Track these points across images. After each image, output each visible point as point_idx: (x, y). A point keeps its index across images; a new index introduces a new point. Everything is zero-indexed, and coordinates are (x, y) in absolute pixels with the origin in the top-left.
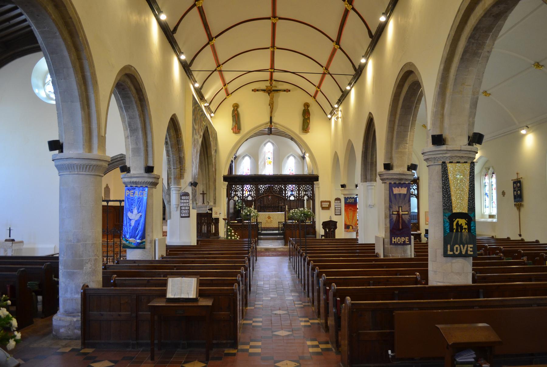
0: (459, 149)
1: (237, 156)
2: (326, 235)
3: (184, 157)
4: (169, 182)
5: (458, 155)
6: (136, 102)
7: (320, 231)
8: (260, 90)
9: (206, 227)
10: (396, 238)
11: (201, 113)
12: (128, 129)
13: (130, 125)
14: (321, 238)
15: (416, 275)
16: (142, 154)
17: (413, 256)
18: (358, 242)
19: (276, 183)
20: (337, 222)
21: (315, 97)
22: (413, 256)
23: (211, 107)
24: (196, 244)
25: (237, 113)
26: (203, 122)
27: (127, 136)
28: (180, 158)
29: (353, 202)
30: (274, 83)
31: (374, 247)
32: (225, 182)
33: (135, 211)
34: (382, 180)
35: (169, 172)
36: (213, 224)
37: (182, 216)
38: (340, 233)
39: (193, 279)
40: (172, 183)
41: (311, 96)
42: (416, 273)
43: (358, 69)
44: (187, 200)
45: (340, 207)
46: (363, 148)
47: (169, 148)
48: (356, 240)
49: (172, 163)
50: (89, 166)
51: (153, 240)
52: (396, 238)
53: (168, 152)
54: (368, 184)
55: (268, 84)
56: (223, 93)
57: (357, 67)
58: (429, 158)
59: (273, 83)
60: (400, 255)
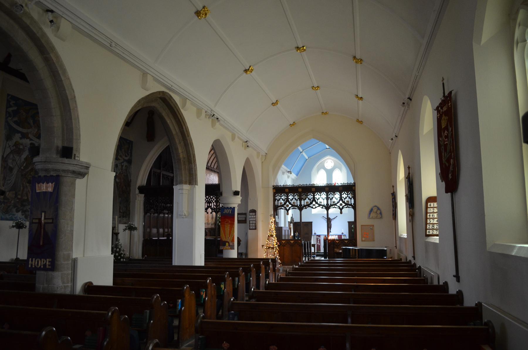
10: (34, 259)
29: (230, 213)
37: (250, 228)
44: (254, 216)
45: (255, 220)
52: (34, 259)
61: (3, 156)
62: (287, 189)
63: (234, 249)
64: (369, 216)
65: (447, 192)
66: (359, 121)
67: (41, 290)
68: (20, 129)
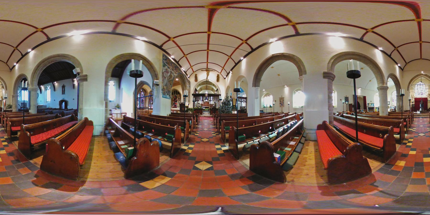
28: (156, 74)
61: (162, 72)
62: (271, 141)
63: (46, 106)
65: (38, 85)
67: (85, 108)
68: (167, 65)
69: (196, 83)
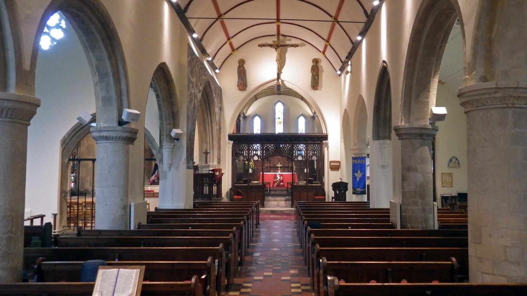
0: (516, 86)
1: (247, 116)
2: (336, 197)
3: (178, 112)
4: (162, 139)
5: (514, 94)
6: (103, 40)
7: (330, 193)
8: (267, 46)
9: (207, 188)
11: (200, 66)
12: (97, 73)
13: (98, 69)
14: (332, 200)
15: (451, 260)
16: (115, 104)
17: (436, 228)
18: (369, 207)
19: (283, 142)
20: (348, 183)
21: (324, 53)
22: (436, 228)
23: (215, 62)
24: (192, 208)
25: (242, 69)
26: (204, 76)
27: (96, 83)
28: (173, 113)
30: (281, 38)
31: (389, 213)
32: (230, 141)
33: (359, 172)
34: (398, 135)
35: (161, 128)
36: (206, 184)
38: (350, 197)
39: (134, 271)
40: (165, 140)
41: (320, 51)
42: (451, 258)
43: (370, 15)
46: (375, 102)
47: (160, 101)
48: (368, 203)
49: (164, 118)
50: (6, 110)
51: (127, 205)
53: (159, 106)
54: (381, 141)
55: (275, 39)
56: (227, 49)
57: (369, 12)
58: (469, 101)
59: (280, 38)
60: (420, 226)
64: (449, 166)
66: (442, 83)
69: (244, 94)
